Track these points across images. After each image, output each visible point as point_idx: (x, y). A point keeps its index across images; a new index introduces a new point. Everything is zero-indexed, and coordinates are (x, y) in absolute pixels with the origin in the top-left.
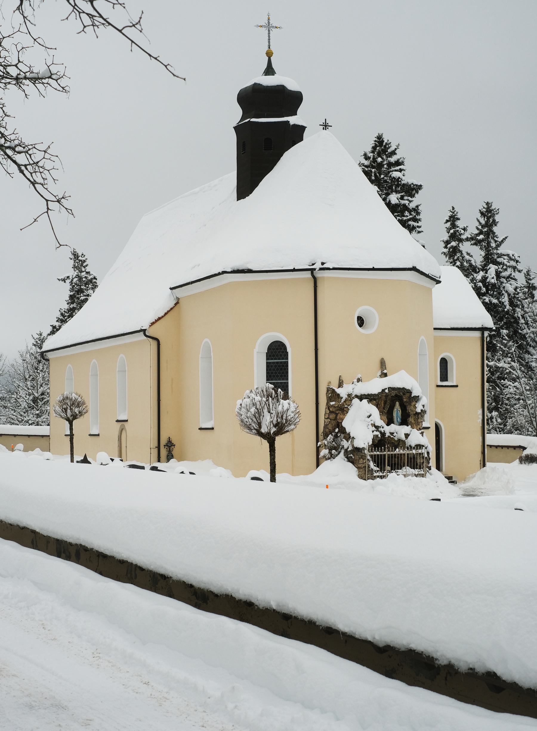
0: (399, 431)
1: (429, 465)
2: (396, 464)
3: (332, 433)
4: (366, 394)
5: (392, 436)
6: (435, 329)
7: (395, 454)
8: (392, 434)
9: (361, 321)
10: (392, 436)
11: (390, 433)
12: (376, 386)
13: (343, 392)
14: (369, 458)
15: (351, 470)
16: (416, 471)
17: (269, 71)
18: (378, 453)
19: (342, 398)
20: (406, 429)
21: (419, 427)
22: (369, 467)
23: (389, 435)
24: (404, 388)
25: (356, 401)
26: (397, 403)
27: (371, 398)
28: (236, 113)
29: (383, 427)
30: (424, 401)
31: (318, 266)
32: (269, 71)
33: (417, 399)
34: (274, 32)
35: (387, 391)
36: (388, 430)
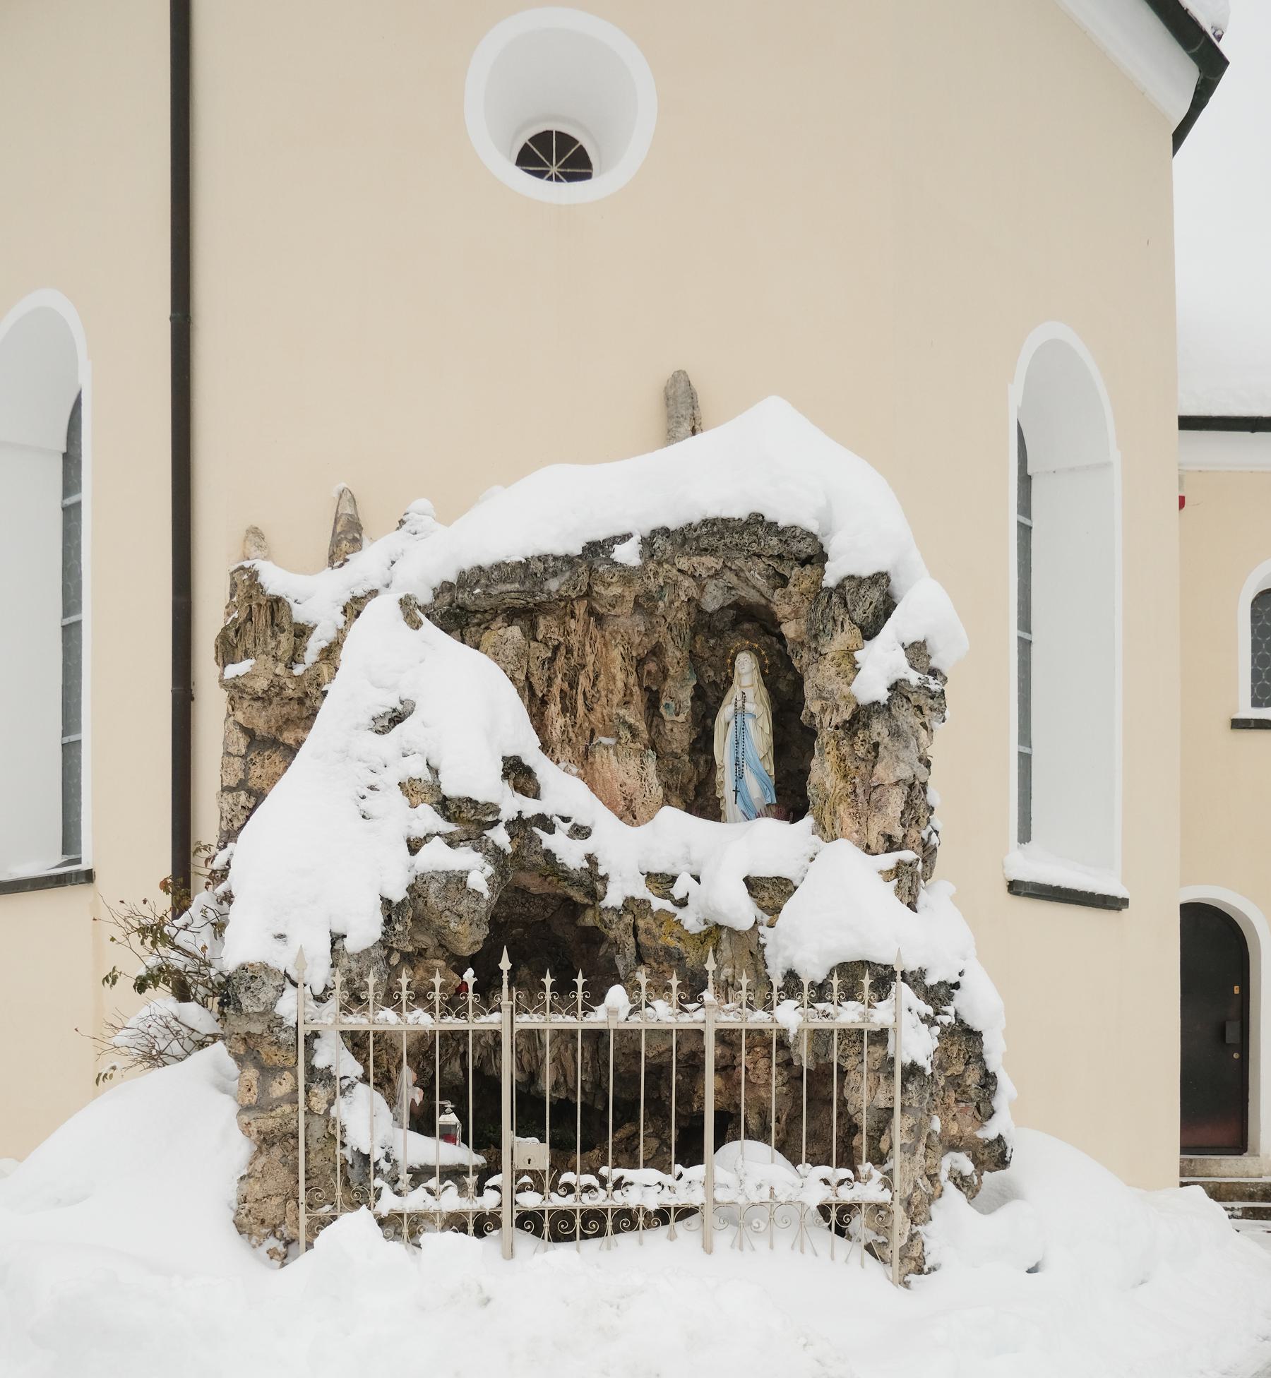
0: (710, 860)
1: (990, 1132)
2: (631, 1113)
4: (452, 578)
5: (658, 904)
6: (1187, 423)
7: (596, 1037)
8: (662, 882)
9: (555, 154)
10: (658, 904)
11: (650, 877)
14: (333, 1055)
16: (813, 1184)
18: (421, 1020)
19: (302, 632)
20: (774, 844)
21: (877, 826)
22: (332, 1135)
23: (640, 890)
24: (757, 520)
26: (746, 667)
29: (581, 832)
30: (921, 610)
33: (873, 603)
35: (627, 554)
36: (627, 847)
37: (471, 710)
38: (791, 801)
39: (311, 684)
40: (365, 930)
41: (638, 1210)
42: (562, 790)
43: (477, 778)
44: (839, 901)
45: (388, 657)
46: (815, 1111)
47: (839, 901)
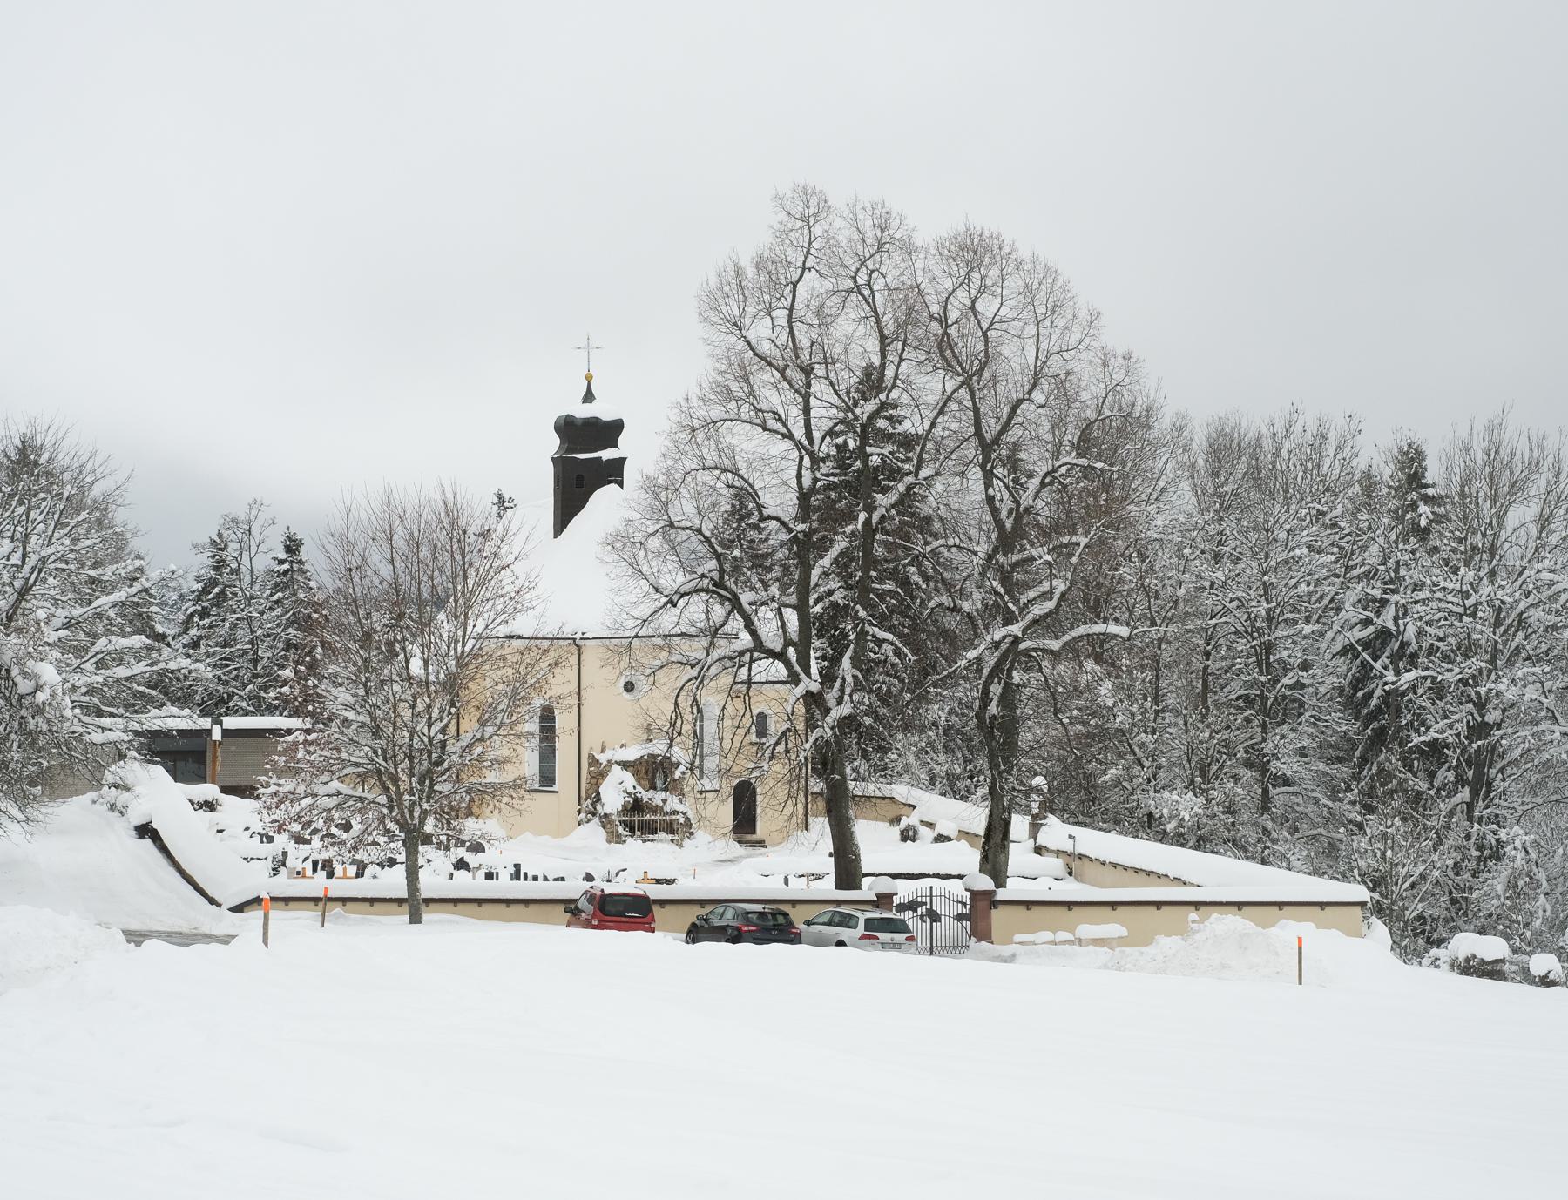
0: (658, 797)
2: (648, 829)
3: (590, 799)
12: (632, 754)
13: (603, 758)
15: (602, 833)
16: (670, 837)
17: (589, 397)
20: (662, 795)
25: (616, 768)
27: (625, 765)
28: (554, 442)
31: (578, 636)
32: (589, 397)
34: (594, 353)
36: (645, 795)
37: (629, 779)
38: (666, 789)
39: (478, 708)
40: (1461, 958)
41: (1534, 466)
42: (639, 789)
43: (631, 790)
44: (673, 803)
45: (617, 773)
46: (670, 828)
47: (673, 803)
